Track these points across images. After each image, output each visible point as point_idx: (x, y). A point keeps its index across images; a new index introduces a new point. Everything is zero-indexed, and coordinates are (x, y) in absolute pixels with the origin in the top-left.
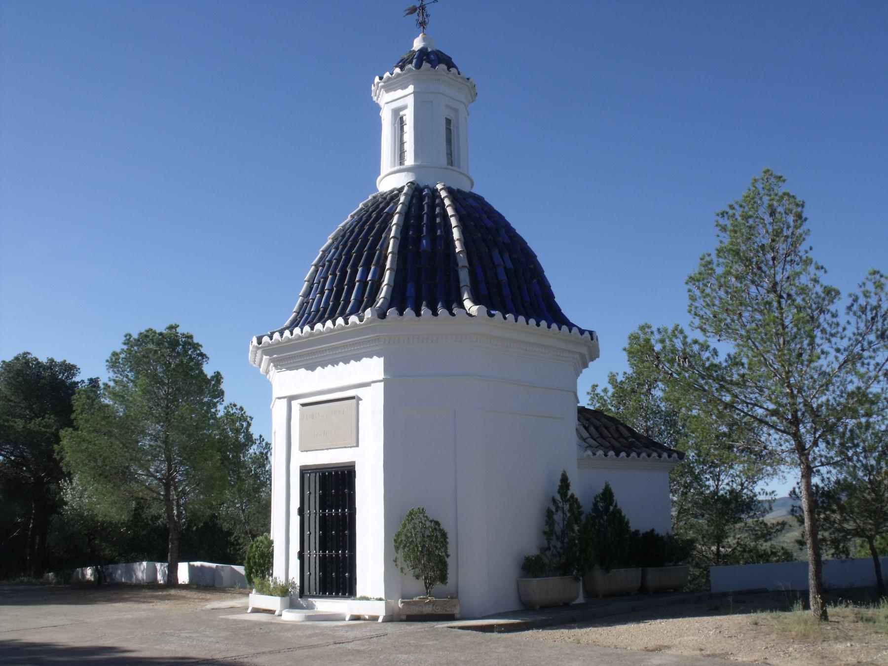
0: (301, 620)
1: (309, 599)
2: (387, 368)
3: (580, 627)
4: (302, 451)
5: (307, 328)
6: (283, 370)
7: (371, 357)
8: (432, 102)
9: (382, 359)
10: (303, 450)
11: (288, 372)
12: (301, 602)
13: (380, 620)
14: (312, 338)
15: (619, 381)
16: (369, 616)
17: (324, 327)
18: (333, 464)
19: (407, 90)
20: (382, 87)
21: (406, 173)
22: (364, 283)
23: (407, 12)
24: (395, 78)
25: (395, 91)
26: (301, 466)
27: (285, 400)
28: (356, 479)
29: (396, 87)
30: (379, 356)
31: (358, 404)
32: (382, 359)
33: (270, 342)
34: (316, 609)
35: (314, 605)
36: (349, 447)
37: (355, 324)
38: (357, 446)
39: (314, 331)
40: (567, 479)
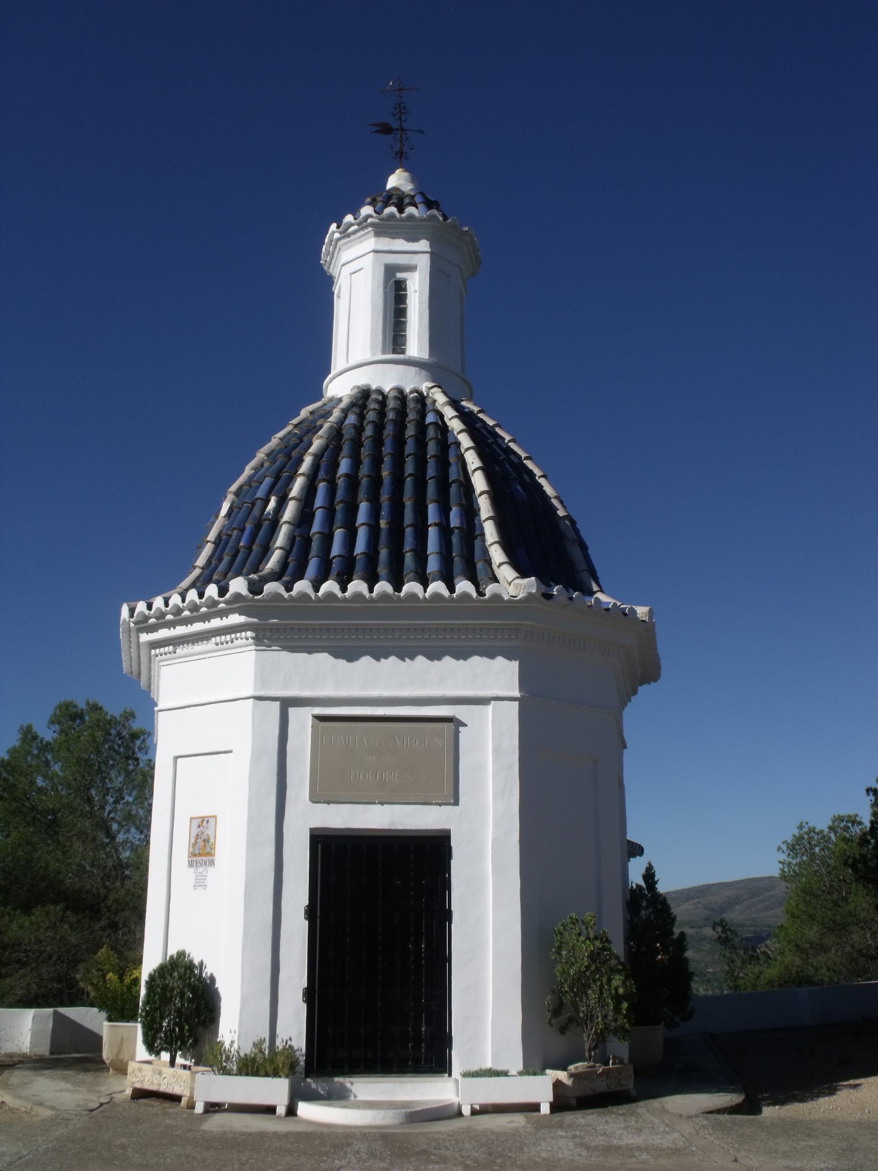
0: (396, 1122)
1: (336, 1079)
2: (523, 682)
3: (802, 1100)
4: (314, 802)
5: (383, 587)
6: (273, 648)
7: (492, 656)
8: (449, 276)
9: (515, 665)
10: (315, 798)
11: (285, 654)
12: (314, 1086)
13: (545, 1109)
14: (358, 605)
15: (108, 720)
16: (481, 1105)
17: (425, 591)
18: (396, 830)
19: (415, 244)
20: (372, 225)
21: (418, 369)
22: (445, 531)
23: (379, 128)
24: (401, 219)
25: (393, 238)
26: (312, 830)
27: (277, 704)
28: (452, 862)
29: (397, 234)
30: (510, 658)
31: (457, 733)
32: (515, 665)
33: (339, 594)
34: (352, 1098)
35: (350, 1091)
36: (437, 804)
37: (465, 596)
38: (456, 803)
39: (402, 594)
40: (653, 875)
